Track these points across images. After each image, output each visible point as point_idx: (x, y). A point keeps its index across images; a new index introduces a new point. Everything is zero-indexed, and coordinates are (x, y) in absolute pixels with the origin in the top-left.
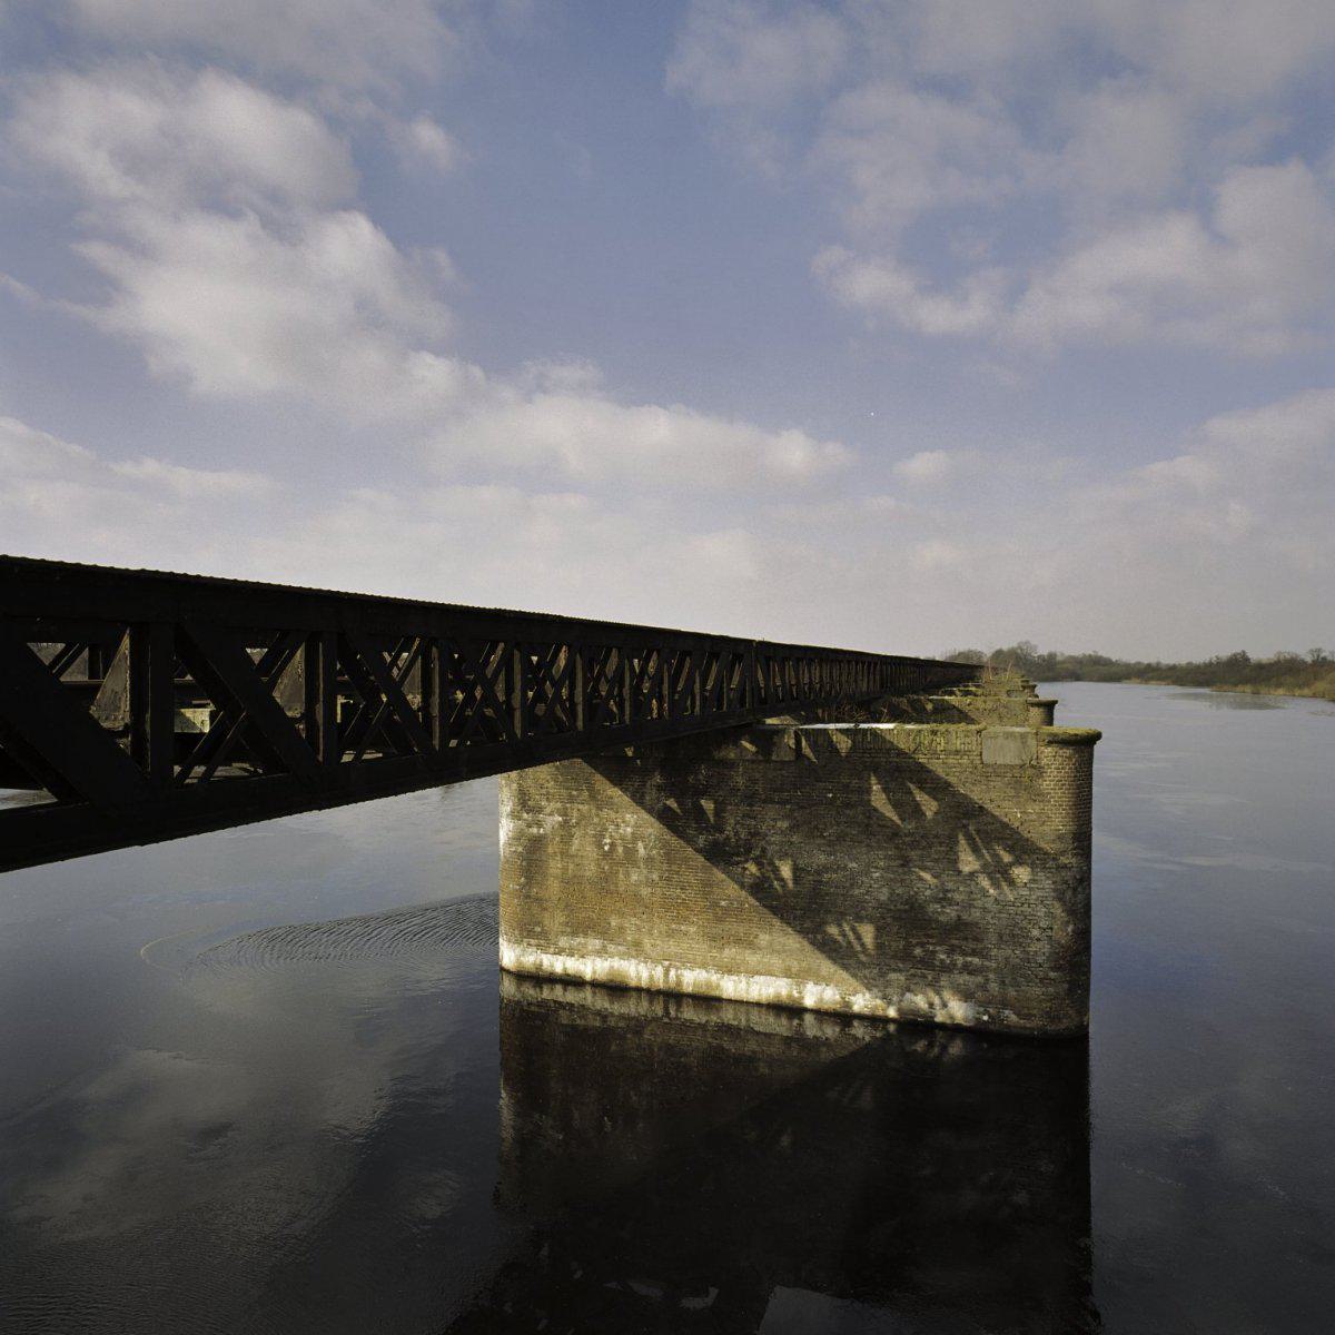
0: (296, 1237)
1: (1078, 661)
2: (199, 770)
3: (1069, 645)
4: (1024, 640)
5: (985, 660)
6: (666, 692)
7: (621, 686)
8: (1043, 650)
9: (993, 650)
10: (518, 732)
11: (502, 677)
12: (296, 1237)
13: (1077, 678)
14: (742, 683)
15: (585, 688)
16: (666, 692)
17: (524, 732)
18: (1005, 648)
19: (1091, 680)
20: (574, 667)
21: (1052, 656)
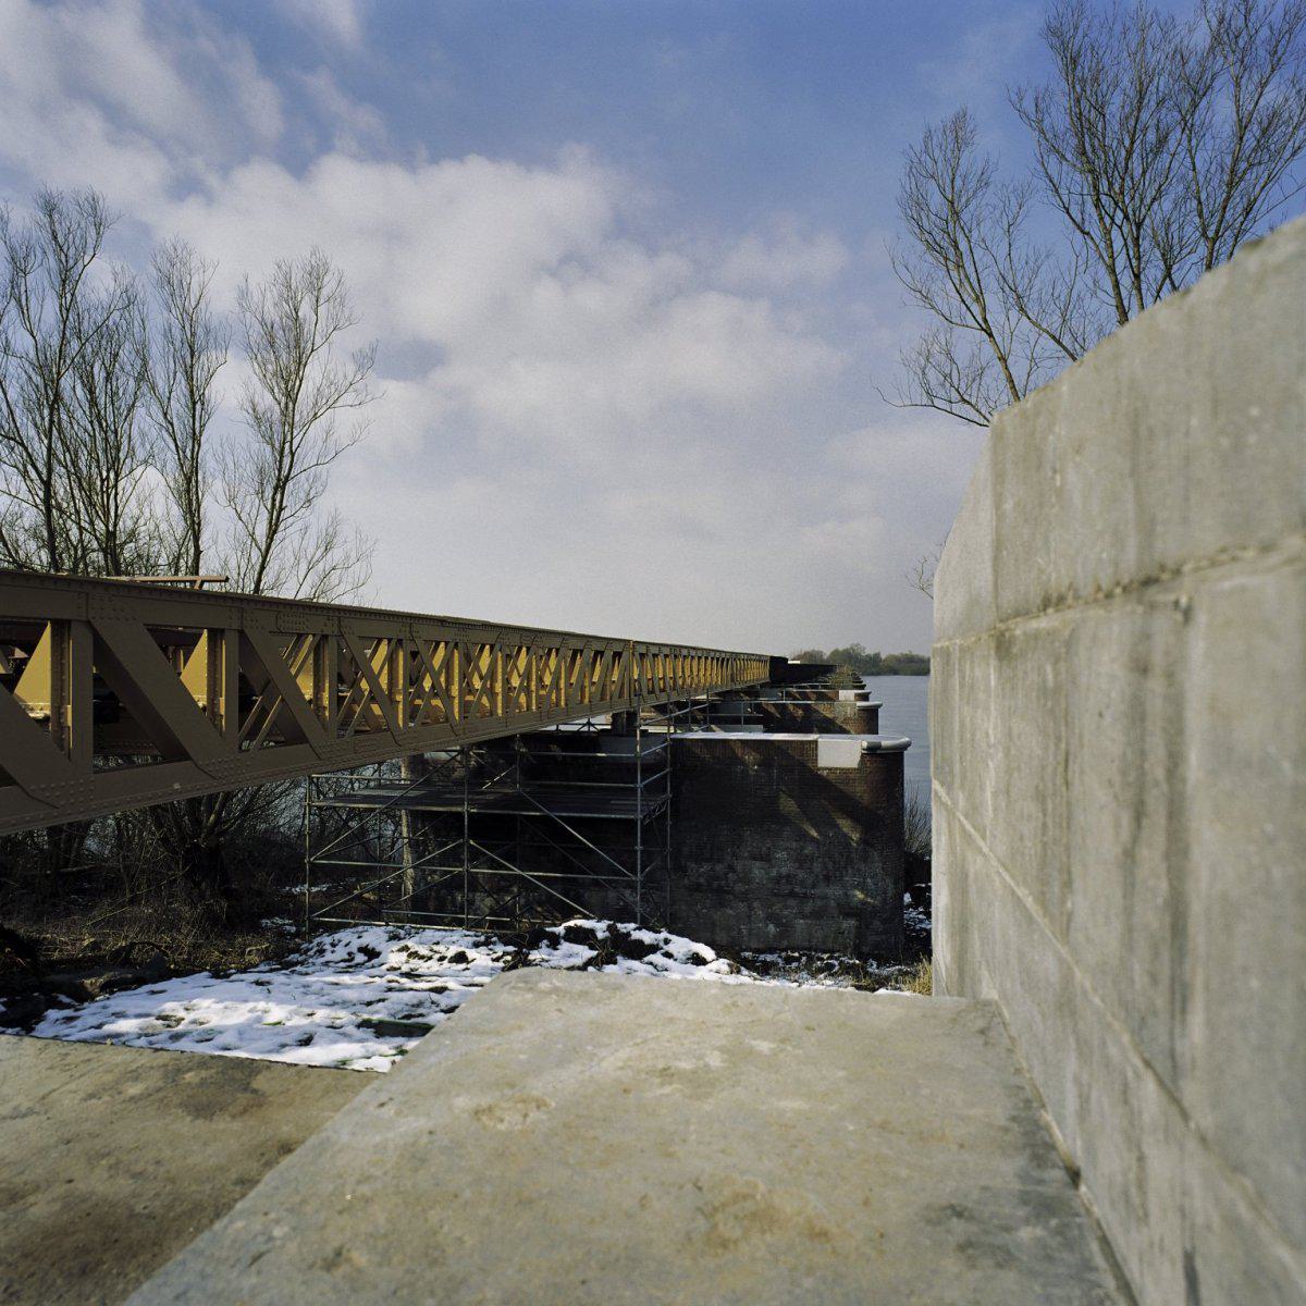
0: (34, 1155)
1: (898, 660)
2: (287, 888)
3: (887, 649)
4: (856, 642)
5: (825, 657)
6: (533, 688)
7: (529, 681)
8: (870, 651)
9: (832, 650)
10: (401, 723)
11: (385, 671)
12: (34, 1155)
13: (895, 672)
14: (622, 677)
15: (460, 685)
16: (533, 688)
17: (405, 723)
18: (841, 649)
19: (905, 675)
20: (496, 667)
21: (877, 656)
